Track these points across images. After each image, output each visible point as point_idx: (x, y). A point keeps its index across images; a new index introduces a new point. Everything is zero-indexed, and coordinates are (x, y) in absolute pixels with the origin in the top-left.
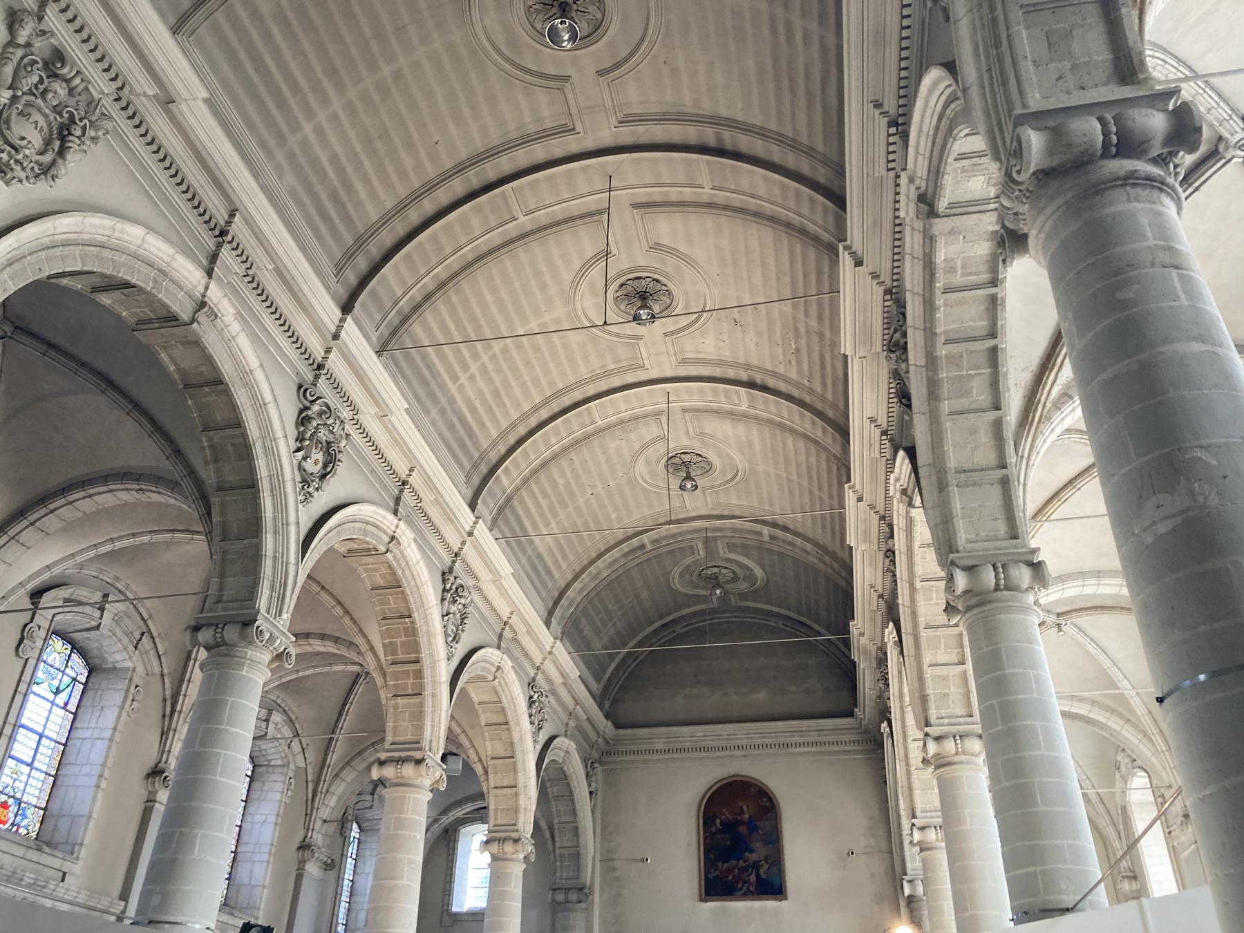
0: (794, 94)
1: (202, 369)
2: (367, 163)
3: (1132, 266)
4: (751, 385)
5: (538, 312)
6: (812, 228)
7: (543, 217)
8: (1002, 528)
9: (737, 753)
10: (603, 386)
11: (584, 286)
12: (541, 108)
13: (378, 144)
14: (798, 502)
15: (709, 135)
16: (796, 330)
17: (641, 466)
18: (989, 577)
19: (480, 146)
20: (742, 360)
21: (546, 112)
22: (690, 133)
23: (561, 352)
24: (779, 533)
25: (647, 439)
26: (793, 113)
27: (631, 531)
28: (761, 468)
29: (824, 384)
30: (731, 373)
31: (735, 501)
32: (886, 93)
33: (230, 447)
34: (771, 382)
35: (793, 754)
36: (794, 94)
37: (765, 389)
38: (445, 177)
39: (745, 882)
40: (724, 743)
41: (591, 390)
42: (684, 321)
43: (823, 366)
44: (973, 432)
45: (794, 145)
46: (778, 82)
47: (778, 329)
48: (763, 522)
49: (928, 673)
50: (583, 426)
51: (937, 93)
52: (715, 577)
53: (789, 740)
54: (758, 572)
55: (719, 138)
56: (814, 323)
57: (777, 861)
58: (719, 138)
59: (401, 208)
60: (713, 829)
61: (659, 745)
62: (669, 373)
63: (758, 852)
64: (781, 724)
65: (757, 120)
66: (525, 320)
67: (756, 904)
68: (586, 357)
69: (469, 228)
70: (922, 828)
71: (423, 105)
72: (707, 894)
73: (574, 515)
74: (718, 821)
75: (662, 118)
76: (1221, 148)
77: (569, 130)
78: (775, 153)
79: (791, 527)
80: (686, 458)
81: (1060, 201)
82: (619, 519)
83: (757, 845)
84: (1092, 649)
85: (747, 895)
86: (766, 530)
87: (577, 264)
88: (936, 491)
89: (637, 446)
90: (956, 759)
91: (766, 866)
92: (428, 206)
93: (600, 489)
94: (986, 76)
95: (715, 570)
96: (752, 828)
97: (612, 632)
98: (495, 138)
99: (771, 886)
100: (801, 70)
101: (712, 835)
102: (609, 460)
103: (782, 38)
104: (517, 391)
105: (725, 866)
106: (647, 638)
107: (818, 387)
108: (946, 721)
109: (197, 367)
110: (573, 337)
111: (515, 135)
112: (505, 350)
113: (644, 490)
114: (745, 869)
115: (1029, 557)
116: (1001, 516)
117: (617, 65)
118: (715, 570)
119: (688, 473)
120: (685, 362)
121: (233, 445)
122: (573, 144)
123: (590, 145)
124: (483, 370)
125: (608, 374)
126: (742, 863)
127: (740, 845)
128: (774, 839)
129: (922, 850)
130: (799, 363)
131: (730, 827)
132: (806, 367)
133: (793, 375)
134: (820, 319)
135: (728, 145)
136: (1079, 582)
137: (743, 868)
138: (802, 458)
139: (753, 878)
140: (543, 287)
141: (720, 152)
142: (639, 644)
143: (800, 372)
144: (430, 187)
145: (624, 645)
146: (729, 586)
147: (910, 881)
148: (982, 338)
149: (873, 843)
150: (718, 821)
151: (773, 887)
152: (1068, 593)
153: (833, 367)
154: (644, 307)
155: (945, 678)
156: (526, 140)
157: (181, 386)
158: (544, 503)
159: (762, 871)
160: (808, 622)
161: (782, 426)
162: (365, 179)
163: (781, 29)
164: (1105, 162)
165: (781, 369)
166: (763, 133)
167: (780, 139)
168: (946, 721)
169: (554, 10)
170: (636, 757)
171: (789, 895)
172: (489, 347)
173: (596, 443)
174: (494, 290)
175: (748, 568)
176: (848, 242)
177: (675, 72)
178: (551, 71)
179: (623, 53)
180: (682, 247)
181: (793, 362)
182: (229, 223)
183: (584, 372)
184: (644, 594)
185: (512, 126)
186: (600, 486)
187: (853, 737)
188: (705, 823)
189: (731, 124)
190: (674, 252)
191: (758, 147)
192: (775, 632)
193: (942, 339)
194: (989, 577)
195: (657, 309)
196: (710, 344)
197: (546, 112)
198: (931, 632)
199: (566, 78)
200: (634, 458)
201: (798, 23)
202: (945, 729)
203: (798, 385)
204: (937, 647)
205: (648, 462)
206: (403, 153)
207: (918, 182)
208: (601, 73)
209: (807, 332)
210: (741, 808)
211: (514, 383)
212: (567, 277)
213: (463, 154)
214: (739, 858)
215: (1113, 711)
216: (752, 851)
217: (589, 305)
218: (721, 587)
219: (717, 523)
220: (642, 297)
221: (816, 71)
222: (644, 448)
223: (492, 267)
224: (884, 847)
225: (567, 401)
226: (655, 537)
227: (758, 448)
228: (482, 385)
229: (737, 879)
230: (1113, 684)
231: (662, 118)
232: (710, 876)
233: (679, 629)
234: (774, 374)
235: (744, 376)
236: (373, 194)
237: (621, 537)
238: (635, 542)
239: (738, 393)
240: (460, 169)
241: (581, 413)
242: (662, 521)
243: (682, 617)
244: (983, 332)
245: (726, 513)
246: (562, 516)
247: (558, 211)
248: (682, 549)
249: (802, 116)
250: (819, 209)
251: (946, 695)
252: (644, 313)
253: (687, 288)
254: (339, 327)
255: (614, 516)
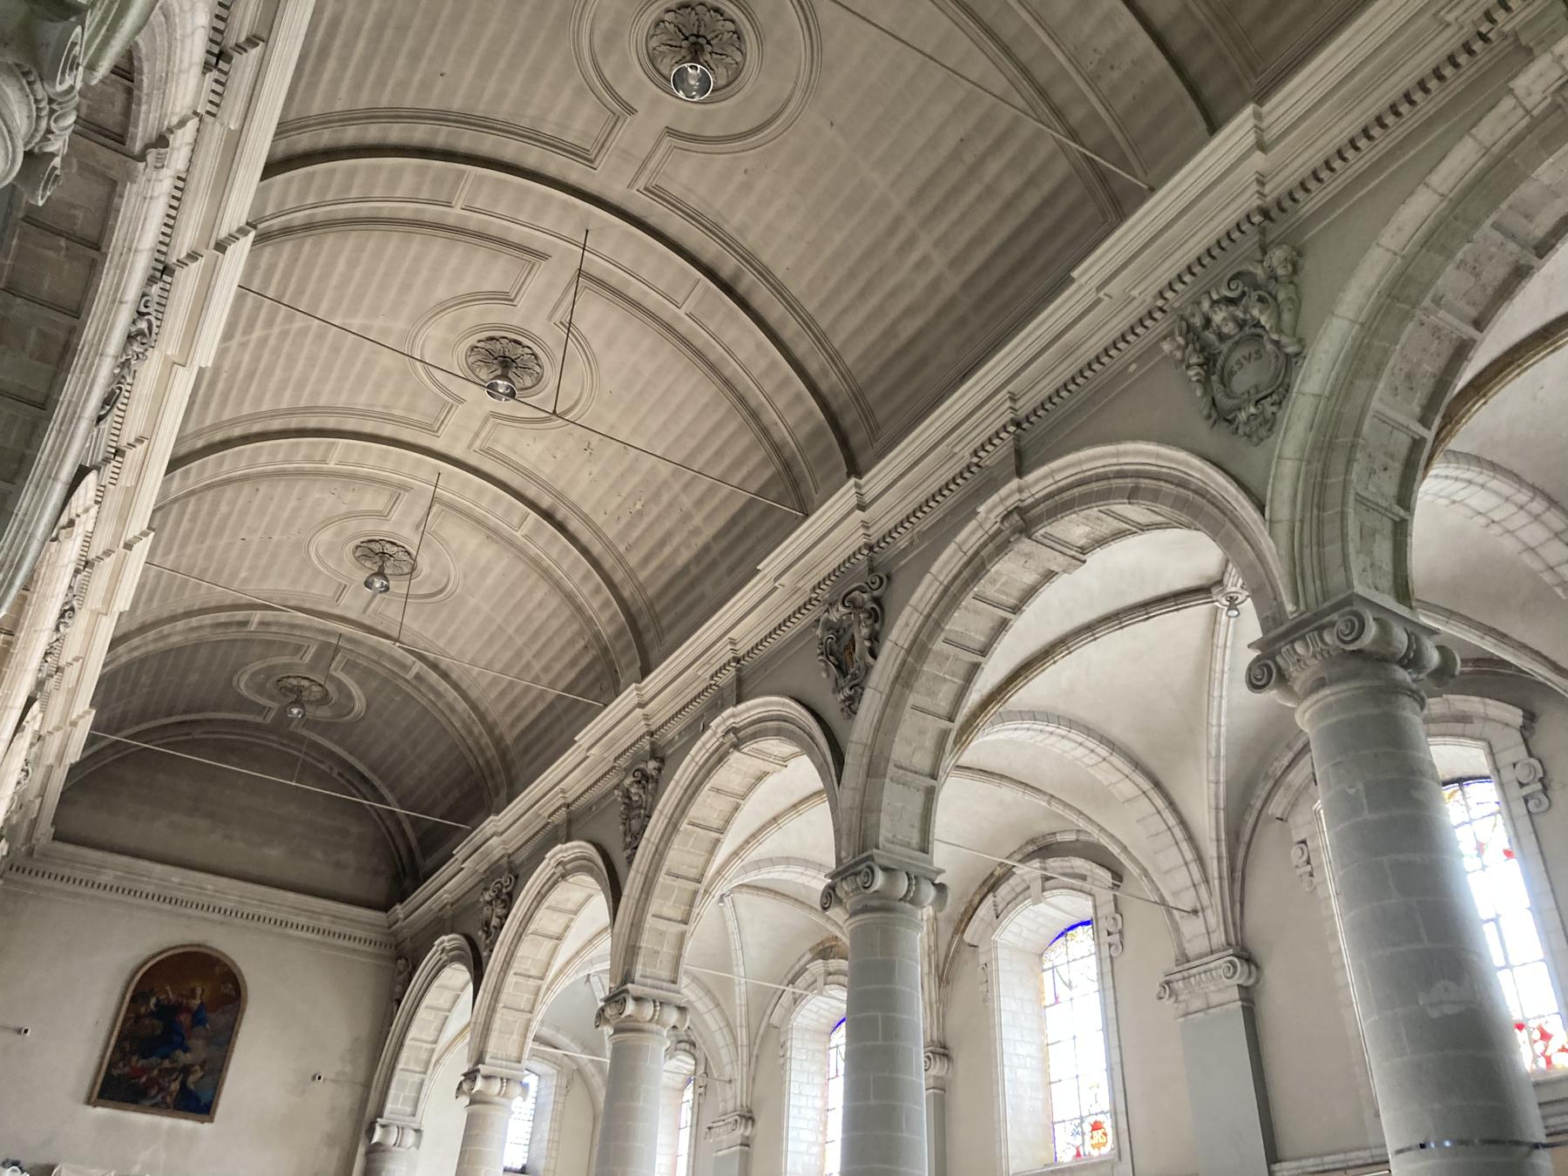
0: (863, 295)
1: (80, 214)
2: (361, 44)
3: (1422, 773)
4: (548, 515)
5: (374, 312)
6: (770, 416)
7: (474, 221)
8: (915, 839)
9: (209, 915)
10: (368, 427)
11: (448, 317)
12: (581, 123)
13: (389, 34)
14: (489, 655)
15: (729, 265)
16: (657, 496)
17: (326, 536)
18: (903, 885)
19: (481, 109)
20: (560, 485)
21: (578, 125)
22: (711, 250)
23: (359, 365)
24: (433, 677)
25: (364, 507)
26: (845, 311)
27: (245, 599)
28: (472, 601)
29: (646, 560)
30: (531, 492)
31: (421, 627)
32: (1029, 395)
33: (33, 336)
34: (574, 525)
35: (290, 937)
36: (863, 295)
37: (561, 527)
38: (417, 116)
39: (161, 1090)
40: (206, 901)
41: (350, 424)
42: (526, 412)
43: (662, 543)
44: (922, 732)
45: (821, 339)
46: (852, 274)
47: (633, 481)
48: (421, 658)
49: (650, 922)
50: (308, 459)
51: (1152, 461)
52: (299, 690)
53: (294, 919)
54: (360, 704)
55: (738, 275)
56: (687, 502)
57: (216, 1070)
58: (738, 275)
59: (349, 118)
60: (143, 1010)
61: (107, 877)
62: (457, 453)
63: (196, 1052)
64: (291, 896)
65: (796, 288)
66: (352, 311)
67: (166, 1122)
68: (379, 387)
69: (397, 183)
70: (487, 1077)
71: (466, 27)
72: (100, 1096)
73: (202, 554)
74: (153, 1000)
75: (693, 217)
76: (1215, 591)
77: (584, 157)
78: (790, 329)
79: (454, 676)
80: (390, 549)
81: (1366, 683)
82: (246, 580)
83: (197, 1044)
84: (732, 925)
85: (160, 1108)
86: (418, 667)
87: (464, 288)
88: (862, 773)
89: (344, 509)
90: (647, 1026)
91: (200, 1074)
92: (373, 133)
93: (256, 538)
94: (1297, 524)
95: (305, 683)
96: (198, 1018)
97: (119, 710)
98: (503, 112)
99: (197, 1102)
100: (890, 284)
101: (138, 1018)
102: (296, 510)
103: (895, 244)
104: (273, 385)
105: (142, 1062)
106: (147, 731)
107: (633, 560)
108: (649, 981)
109: (74, 207)
110: (387, 359)
111: (525, 123)
112: (303, 332)
113: (306, 561)
114: (169, 1071)
115: (932, 876)
116: (917, 824)
117: (693, 138)
118: (305, 683)
119: (382, 568)
120: (488, 452)
121: (42, 334)
122: (575, 173)
123: (592, 186)
124: (263, 341)
125: (386, 418)
126: (167, 1063)
127: (168, 1044)
128: (224, 1042)
129: (472, 1102)
130: (630, 525)
131: (167, 1012)
132: (635, 534)
133: (611, 533)
134: (699, 503)
135: (741, 288)
136: (800, 869)
137: (167, 1070)
138: (542, 615)
139: (175, 1086)
140: (406, 287)
141: (728, 288)
142: (133, 737)
143: (622, 535)
144: (396, 115)
145: (116, 731)
146: (309, 708)
147: (383, 1126)
148: (972, 651)
149: (348, 1069)
150: (153, 1000)
151: (198, 1104)
152: (785, 876)
153: (676, 552)
154: (504, 377)
155: (662, 934)
156: (533, 137)
157: (21, 215)
158: (185, 525)
159: (191, 1079)
160: (377, 783)
161: (546, 574)
162: (343, 62)
163: (901, 235)
164: (1396, 667)
165: (599, 520)
166: (792, 305)
167: (808, 323)
168: (649, 981)
169: (685, 44)
170: (58, 885)
171: (216, 1118)
172: (289, 319)
173: (300, 485)
174: (352, 264)
175: (350, 697)
176: (862, 482)
177: (746, 187)
178: (622, 92)
179: (708, 133)
180: (596, 344)
181: (624, 521)
182: (240, 48)
183: (361, 401)
184: (194, 677)
185: (531, 111)
186: (260, 534)
187: (373, 936)
188: (133, 999)
189: (765, 274)
190: (583, 344)
191: (775, 312)
192: (322, 779)
193: (943, 635)
194: (903, 885)
195: (519, 384)
196: (531, 450)
197: (578, 125)
198: (669, 880)
199: (631, 110)
200: (327, 522)
201: (924, 246)
202: (647, 990)
203: (610, 546)
204: (667, 898)
205: (338, 534)
206: (401, 61)
207: (1025, 495)
208: (670, 132)
209: (671, 504)
210: (193, 991)
211: (278, 373)
212: (441, 293)
213: (456, 105)
214: (164, 1057)
215: (708, 992)
216: (186, 1050)
217: (434, 339)
218: (302, 706)
219: (360, 634)
220: (504, 362)
221: (906, 300)
222: (350, 515)
223: (374, 238)
224: (361, 1077)
225: (313, 422)
226: (267, 619)
227: (490, 581)
228: (247, 358)
229: (152, 1082)
230: (727, 966)
231: (693, 217)
232: (115, 1072)
233: (198, 734)
234: (586, 520)
235: (546, 502)
236: (336, 82)
237: (228, 602)
238: (240, 615)
239: (526, 516)
240: (441, 117)
241: (317, 445)
242: (292, 603)
243: (210, 721)
244: (977, 646)
245: (380, 628)
246: (189, 550)
247: (496, 226)
248: (286, 644)
249: (853, 321)
250: (800, 411)
251: (657, 952)
252: (502, 384)
253: (569, 382)
254: (233, 238)
255: (243, 574)
